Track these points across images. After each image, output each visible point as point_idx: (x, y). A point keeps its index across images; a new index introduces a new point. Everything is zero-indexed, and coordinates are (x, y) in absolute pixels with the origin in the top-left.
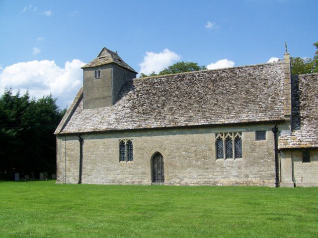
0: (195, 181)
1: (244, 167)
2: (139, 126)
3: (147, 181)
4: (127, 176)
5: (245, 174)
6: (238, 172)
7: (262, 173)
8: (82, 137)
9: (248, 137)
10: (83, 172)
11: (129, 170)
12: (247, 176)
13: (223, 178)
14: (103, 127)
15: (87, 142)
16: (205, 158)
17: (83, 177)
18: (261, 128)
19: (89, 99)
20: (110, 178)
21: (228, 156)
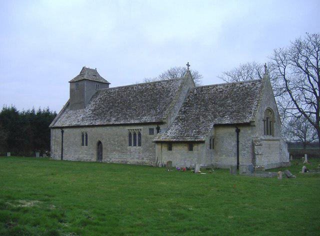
0: (117, 160)
3: (94, 159)
9: (144, 130)
11: (85, 151)
12: (143, 159)
14: (74, 124)
18: (151, 127)
20: (76, 156)
21: (135, 145)
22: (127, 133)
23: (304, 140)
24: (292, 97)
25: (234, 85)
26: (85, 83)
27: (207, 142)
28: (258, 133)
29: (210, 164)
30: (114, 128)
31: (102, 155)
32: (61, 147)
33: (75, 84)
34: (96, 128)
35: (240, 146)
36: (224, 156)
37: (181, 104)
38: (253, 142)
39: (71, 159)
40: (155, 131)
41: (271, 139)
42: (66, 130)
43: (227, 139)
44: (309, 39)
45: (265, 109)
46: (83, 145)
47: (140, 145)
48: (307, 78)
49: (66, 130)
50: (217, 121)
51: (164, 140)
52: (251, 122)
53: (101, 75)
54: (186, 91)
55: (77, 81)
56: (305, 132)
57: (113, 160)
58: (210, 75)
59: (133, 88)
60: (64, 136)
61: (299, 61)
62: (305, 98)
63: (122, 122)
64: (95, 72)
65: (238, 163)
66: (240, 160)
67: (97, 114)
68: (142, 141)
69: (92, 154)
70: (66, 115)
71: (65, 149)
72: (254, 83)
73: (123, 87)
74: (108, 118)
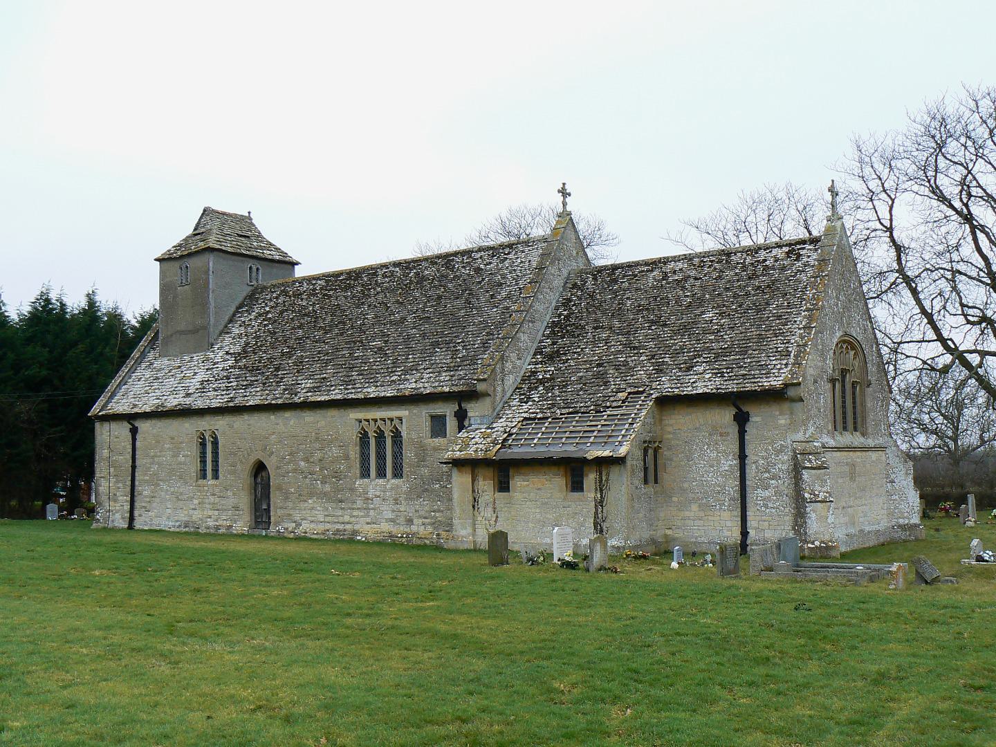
0: (321, 527)
1: (406, 499)
2: (232, 399)
4: (210, 513)
5: (405, 516)
6: (393, 511)
7: (437, 514)
8: (137, 424)
9: (414, 422)
10: (137, 504)
11: (212, 499)
12: (410, 522)
13: (368, 523)
14: (172, 402)
15: (758, 416)
16: (337, 475)
17: (136, 513)
19: (169, 333)
20: (183, 517)
21: (381, 473)
22: (353, 435)
23: (952, 445)
24: (919, 302)
25: (725, 255)
26: (211, 261)
27: (635, 462)
28: (811, 427)
29: (646, 535)
30: (309, 417)
31: (268, 510)
32: (129, 483)
33: (177, 264)
34: (246, 417)
35: (751, 471)
36: (694, 507)
37: (541, 327)
38: (795, 458)
39: (166, 523)
40: (451, 423)
41: (856, 444)
42: (144, 426)
43: (704, 451)
44: (972, 104)
45: (835, 340)
46: (204, 477)
47: (398, 473)
48: (970, 239)
49: (144, 426)
50: (667, 386)
51: (481, 455)
52: (786, 386)
53: (269, 233)
54: (558, 282)
55: (182, 257)
56: (954, 421)
57: (305, 526)
58: (643, 221)
59: (375, 274)
60: (138, 444)
61: (942, 181)
62: (962, 305)
63: (336, 395)
64: (243, 226)
65: (745, 534)
66: (752, 523)
67: (250, 364)
68: (406, 461)
69: (236, 508)
70: (148, 374)
71: (144, 490)
72: (793, 248)
73: (340, 274)
74: (289, 380)
